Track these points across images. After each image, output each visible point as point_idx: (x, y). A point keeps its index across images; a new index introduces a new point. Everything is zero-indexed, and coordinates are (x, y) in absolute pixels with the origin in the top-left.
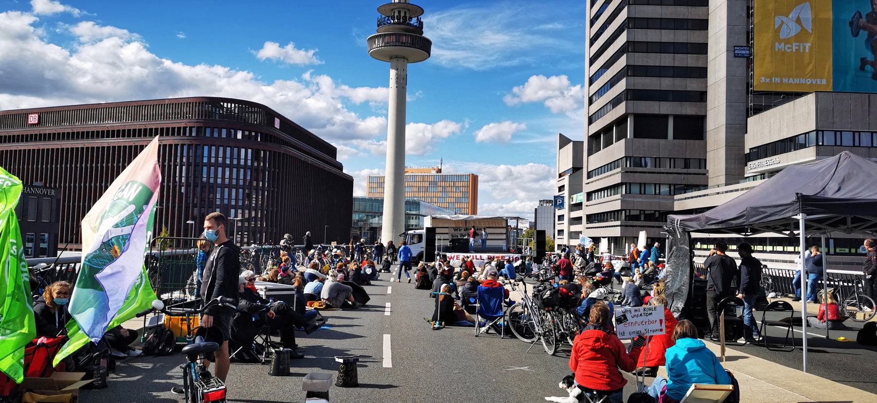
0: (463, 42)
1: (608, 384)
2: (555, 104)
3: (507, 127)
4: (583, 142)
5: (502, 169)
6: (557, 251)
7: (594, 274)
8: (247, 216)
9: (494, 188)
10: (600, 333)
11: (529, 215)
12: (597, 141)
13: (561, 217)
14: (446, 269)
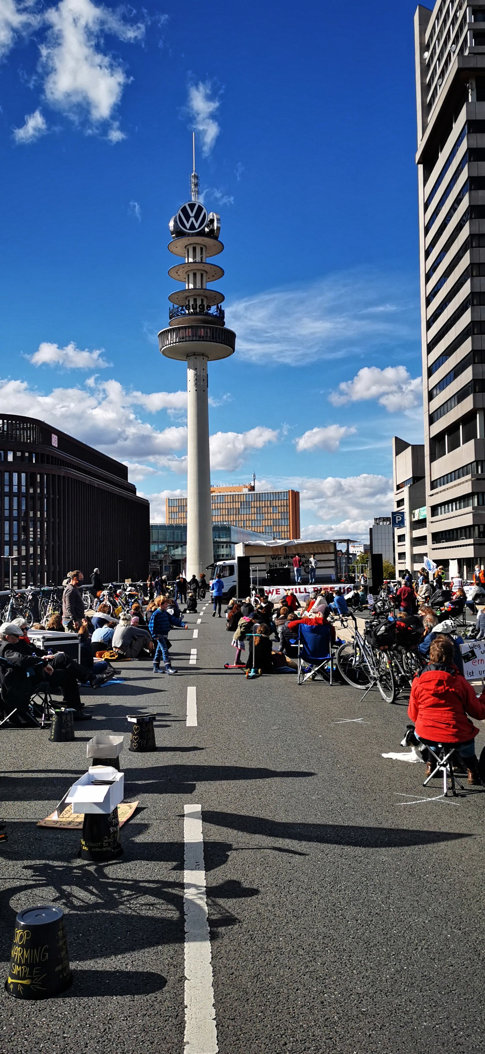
0: (276, 334)
1: (455, 735)
2: (391, 401)
3: (334, 432)
4: (423, 446)
5: (330, 481)
6: (398, 578)
7: (441, 604)
8: (24, 553)
9: (321, 506)
10: (443, 674)
11: (364, 537)
12: (438, 445)
13: (402, 538)
14: (264, 605)
